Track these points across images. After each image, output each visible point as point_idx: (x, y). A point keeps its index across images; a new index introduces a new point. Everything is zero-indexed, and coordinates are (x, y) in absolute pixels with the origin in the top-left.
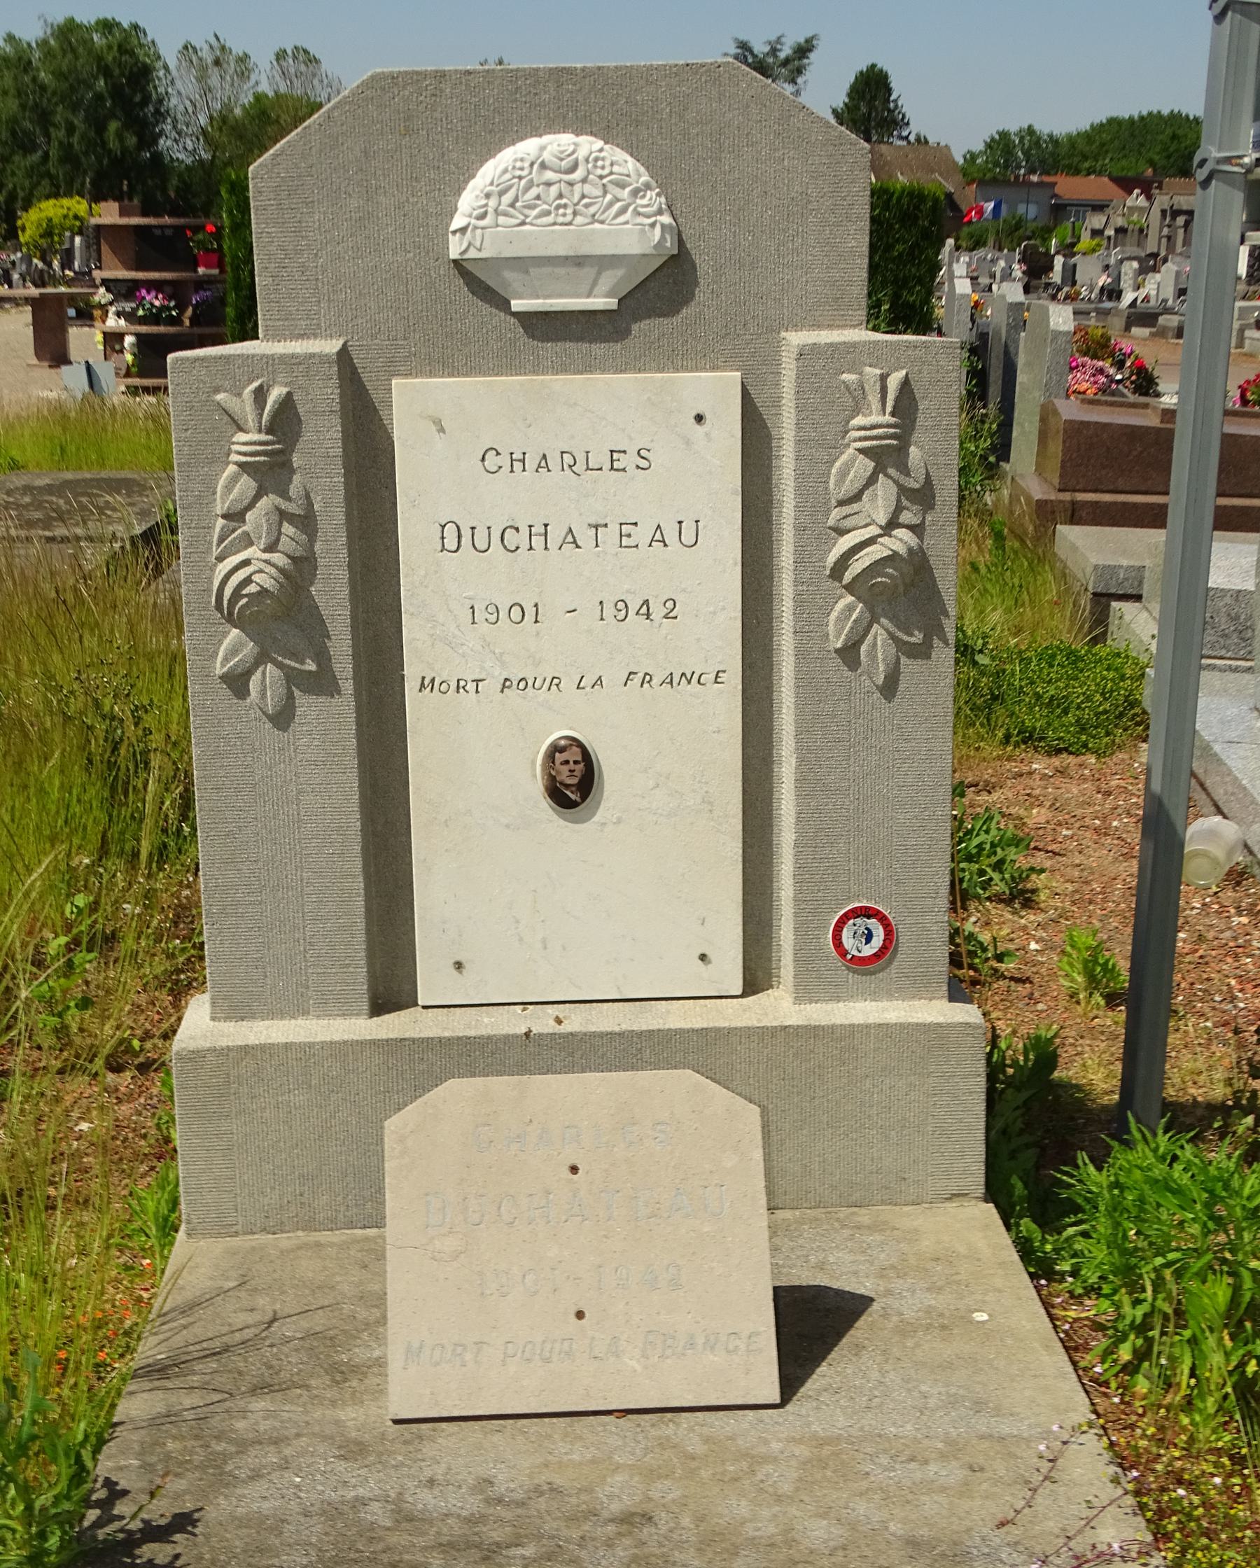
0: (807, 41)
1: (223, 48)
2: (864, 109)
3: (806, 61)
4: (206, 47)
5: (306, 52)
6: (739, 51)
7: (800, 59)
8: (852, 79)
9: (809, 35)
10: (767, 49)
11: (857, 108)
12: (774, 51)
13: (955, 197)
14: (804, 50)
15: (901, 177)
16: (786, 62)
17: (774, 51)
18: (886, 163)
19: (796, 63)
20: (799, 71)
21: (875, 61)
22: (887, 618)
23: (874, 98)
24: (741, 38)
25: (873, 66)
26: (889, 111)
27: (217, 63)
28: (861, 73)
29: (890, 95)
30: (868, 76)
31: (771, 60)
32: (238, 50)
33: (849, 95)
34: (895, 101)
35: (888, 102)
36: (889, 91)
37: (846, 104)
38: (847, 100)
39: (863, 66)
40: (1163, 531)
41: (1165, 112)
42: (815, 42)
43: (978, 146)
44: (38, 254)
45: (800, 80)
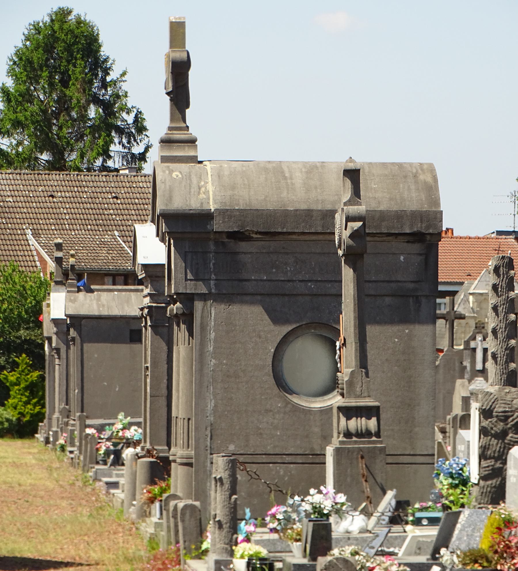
15: (32, 241)
25: (62, 14)
28: (37, 28)
29: (106, 72)
39: (42, 15)
41: (105, 51)
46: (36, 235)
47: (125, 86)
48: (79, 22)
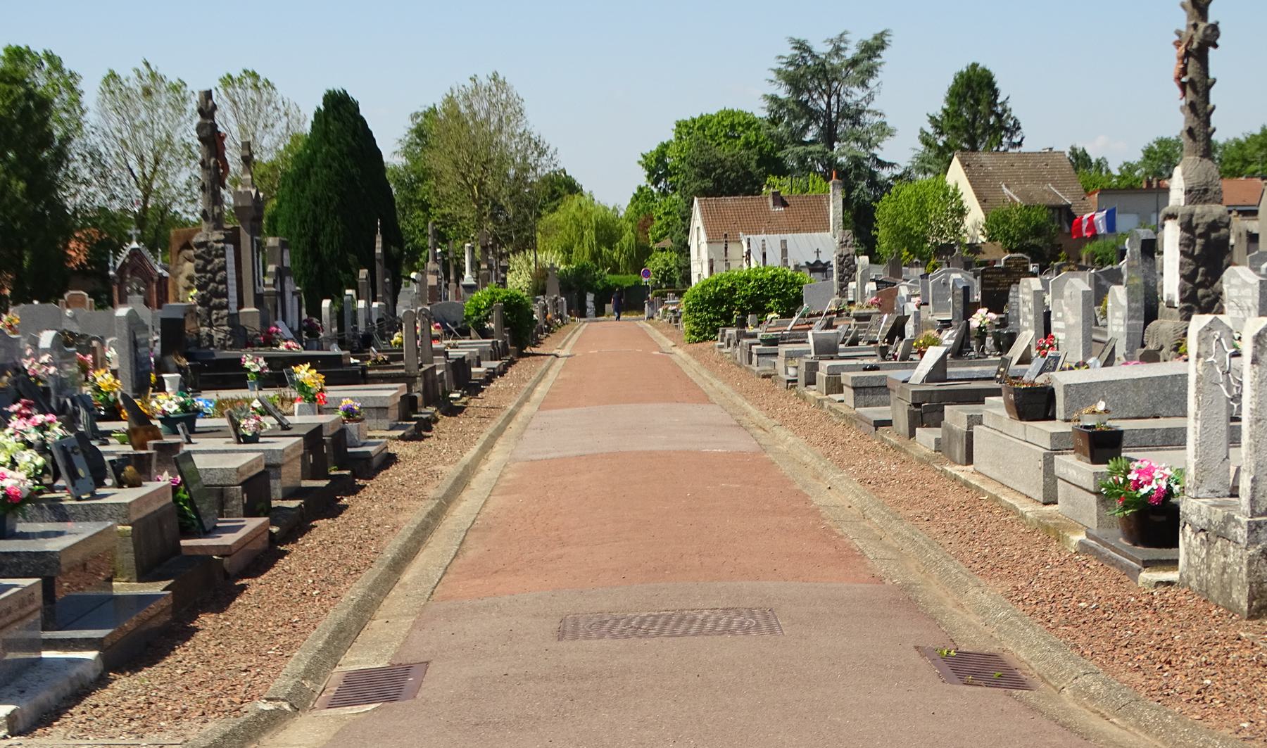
0: (876, 38)
1: (153, 75)
2: (966, 115)
3: (877, 60)
4: (134, 75)
5: (254, 75)
6: (796, 52)
7: (869, 58)
8: (951, 82)
9: (879, 31)
10: (829, 48)
11: (957, 114)
12: (838, 51)
13: (1073, 209)
14: (873, 48)
16: (854, 63)
17: (838, 51)
18: (987, 175)
19: (865, 62)
20: (870, 72)
21: (976, 61)
22: (22, 264)
23: (978, 102)
24: (797, 38)
25: (974, 66)
26: (999, 116)
27: (147, 92)
28: (961, 75)
29: (996, 97)
30: (969, 77)
31: (835, 61)
32: (172, 78)
33: (947, 100)
34: (1002, 103)
35: (996, 105)
36: (995, 93)
37: (945, 110)
38: (946, 106)
40: (939, 430)
42: (886, 39)
43: (1136, 157)
44: (35, 411)
45: (872, 83)
46: (1007, 186)
47: (1009, 106)
48: (984, 70)
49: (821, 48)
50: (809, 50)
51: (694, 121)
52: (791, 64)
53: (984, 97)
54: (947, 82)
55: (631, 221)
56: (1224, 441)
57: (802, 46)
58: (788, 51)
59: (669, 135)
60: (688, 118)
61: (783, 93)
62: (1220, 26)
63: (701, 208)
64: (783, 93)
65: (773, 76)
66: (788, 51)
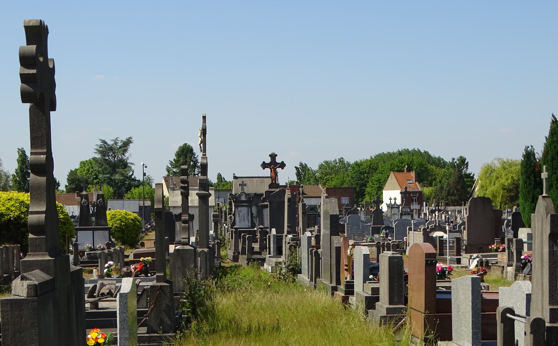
10: (113, 142)
12: (116, 143)
14: (127, 143)
20: (125, 151)
25: (186, 144)
45: (127, 155)
49: (110, 143)
50: (106, 143)
51: (86, 161)
52: (100, 148)
53: (189, 155)
54: (176, 149)
55: (121, 182)
56: (533, 297)
57: (104, 142)
58: (100, 143)
59: (78, 167)
60: (84, 160)
61: (98, 156)
62: (469, 164)
63: (34, 238)
64: (98, 156)
65: (96, 151)
66: (100, 143)
